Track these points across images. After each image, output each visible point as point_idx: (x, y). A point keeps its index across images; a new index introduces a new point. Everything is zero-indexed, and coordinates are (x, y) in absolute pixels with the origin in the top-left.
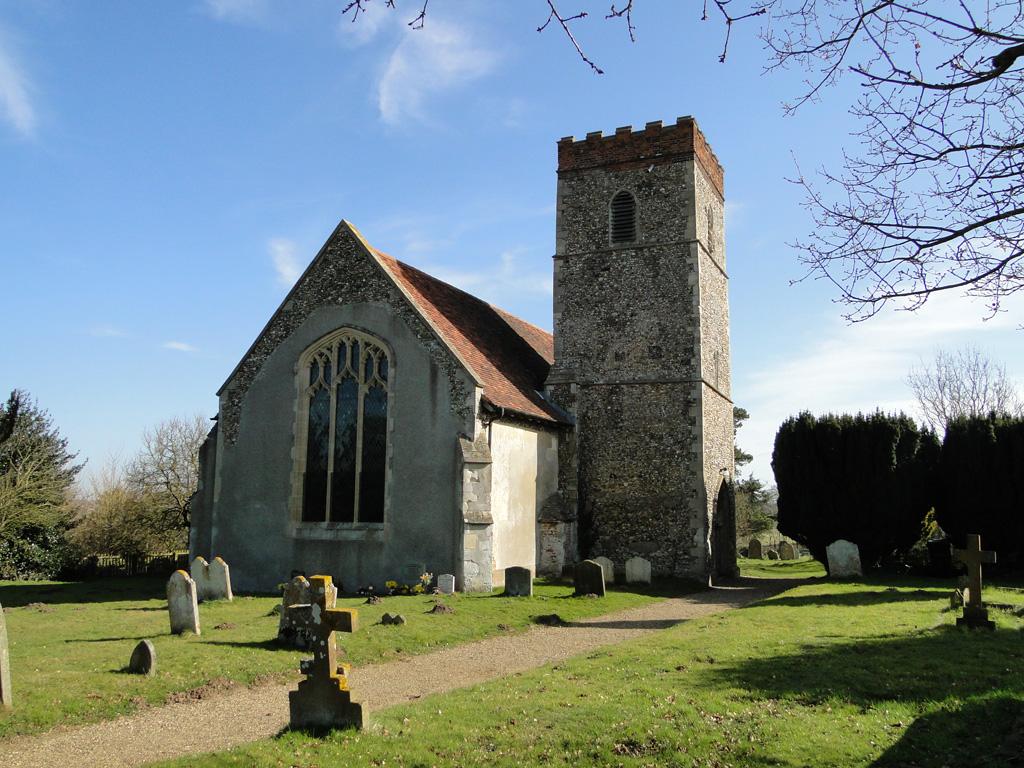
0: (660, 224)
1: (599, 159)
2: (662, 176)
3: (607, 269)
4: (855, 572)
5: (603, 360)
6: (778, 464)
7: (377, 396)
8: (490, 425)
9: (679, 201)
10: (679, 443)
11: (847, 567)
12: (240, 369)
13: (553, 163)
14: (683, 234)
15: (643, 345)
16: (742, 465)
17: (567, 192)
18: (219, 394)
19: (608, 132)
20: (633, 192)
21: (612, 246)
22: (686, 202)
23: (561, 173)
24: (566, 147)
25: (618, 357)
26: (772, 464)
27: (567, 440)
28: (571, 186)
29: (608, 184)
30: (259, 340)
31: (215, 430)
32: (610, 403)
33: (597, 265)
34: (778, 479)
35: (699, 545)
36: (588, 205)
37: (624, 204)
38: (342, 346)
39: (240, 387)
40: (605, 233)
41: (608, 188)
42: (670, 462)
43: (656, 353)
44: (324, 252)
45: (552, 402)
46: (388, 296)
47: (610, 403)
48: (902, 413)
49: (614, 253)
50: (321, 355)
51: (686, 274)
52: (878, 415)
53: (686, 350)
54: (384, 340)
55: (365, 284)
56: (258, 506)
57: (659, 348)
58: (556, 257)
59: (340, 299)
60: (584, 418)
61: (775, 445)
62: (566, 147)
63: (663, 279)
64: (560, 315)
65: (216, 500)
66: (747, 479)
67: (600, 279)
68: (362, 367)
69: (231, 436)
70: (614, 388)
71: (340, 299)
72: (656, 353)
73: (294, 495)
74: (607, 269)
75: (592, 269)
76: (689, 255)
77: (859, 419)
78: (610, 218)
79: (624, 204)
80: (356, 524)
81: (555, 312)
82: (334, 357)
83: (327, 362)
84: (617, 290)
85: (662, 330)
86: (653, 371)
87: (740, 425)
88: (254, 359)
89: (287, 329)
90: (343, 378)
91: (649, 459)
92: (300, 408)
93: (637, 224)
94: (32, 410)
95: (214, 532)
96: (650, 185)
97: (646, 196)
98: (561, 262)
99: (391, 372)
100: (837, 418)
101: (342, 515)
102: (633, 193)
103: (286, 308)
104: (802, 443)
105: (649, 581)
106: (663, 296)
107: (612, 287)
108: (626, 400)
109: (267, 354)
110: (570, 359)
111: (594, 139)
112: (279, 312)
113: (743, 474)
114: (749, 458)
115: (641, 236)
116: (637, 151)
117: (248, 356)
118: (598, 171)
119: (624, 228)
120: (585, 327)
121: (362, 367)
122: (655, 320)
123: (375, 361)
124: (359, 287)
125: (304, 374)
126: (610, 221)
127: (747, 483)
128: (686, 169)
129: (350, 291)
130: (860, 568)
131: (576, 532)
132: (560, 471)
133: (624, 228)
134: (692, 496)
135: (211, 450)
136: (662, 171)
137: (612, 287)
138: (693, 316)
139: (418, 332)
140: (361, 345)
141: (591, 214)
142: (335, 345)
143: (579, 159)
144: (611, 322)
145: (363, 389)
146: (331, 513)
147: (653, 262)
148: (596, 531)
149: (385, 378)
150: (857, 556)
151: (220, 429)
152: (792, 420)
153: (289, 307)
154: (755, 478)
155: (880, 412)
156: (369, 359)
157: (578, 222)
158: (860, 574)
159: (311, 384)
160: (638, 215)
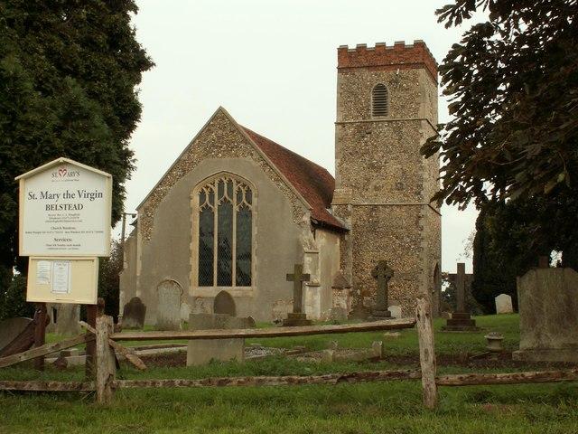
0: (403, 107)
7: (245, 214)
12: (152, 194)
13: (333, 61)
15: (391, 181)
19: (371, 45)
20: (386, 85)
21: (373, 119)
23: (340, 69)
24: (343, 51)
25: (376, 188)
26: (141, 63)
28: (345, 78)
29: (370, 78)
30: (165, 177)
32: (371, 216)
33: (363, 130)
37: (380, 91)
39: (151, 205)
40: (369, 110)
43: (400, 187)
44: (208, 125)
46: (252, 155)
47: (371, 216)
50: (207, 187)
53: (418, 186)
55: (237, 147)
58: (337, 124)
60: (355, 226)
64: (339, 161)
68: (235, 196)
69: (147, 236)
70: (375, 208)
72: (400, 187)
73: (193, 271)
74: (370, 133)
79: (380, 91)
81: (336, 158)
82: (216, 190)
83: (212, 192)
84: (376, 146)
85: (404, 173)
86: (396, 199)
89: (184, 171)
90: (240, 207)
91: (394, 251)
93: (389, 105)
96: (397, 82)
99: (255, 200)
101: (225, 280)
106: (404, 152)
107: (373, 144)
108: (382, 215)
110: (346, 189)
111: (361, 49)
112: (179, 161)
117: (157, 186)
119: (380, 108)
120: (357, 171)
121: (235, 196)
122: (399, 166)
123: (244, 192)
124: (232, 148)
125: (196, 199)
132: (341, 258)
133: (380, 108)
136: (405, 73)
137: (373, 144)
140: (235, 182)
142: (217, 181)
144: (372, 166)
147: (398, 130)
149: (250, 202)
153: (185, 157)
156: (239, 192)
157: (351, 101)
160: (389, 100)
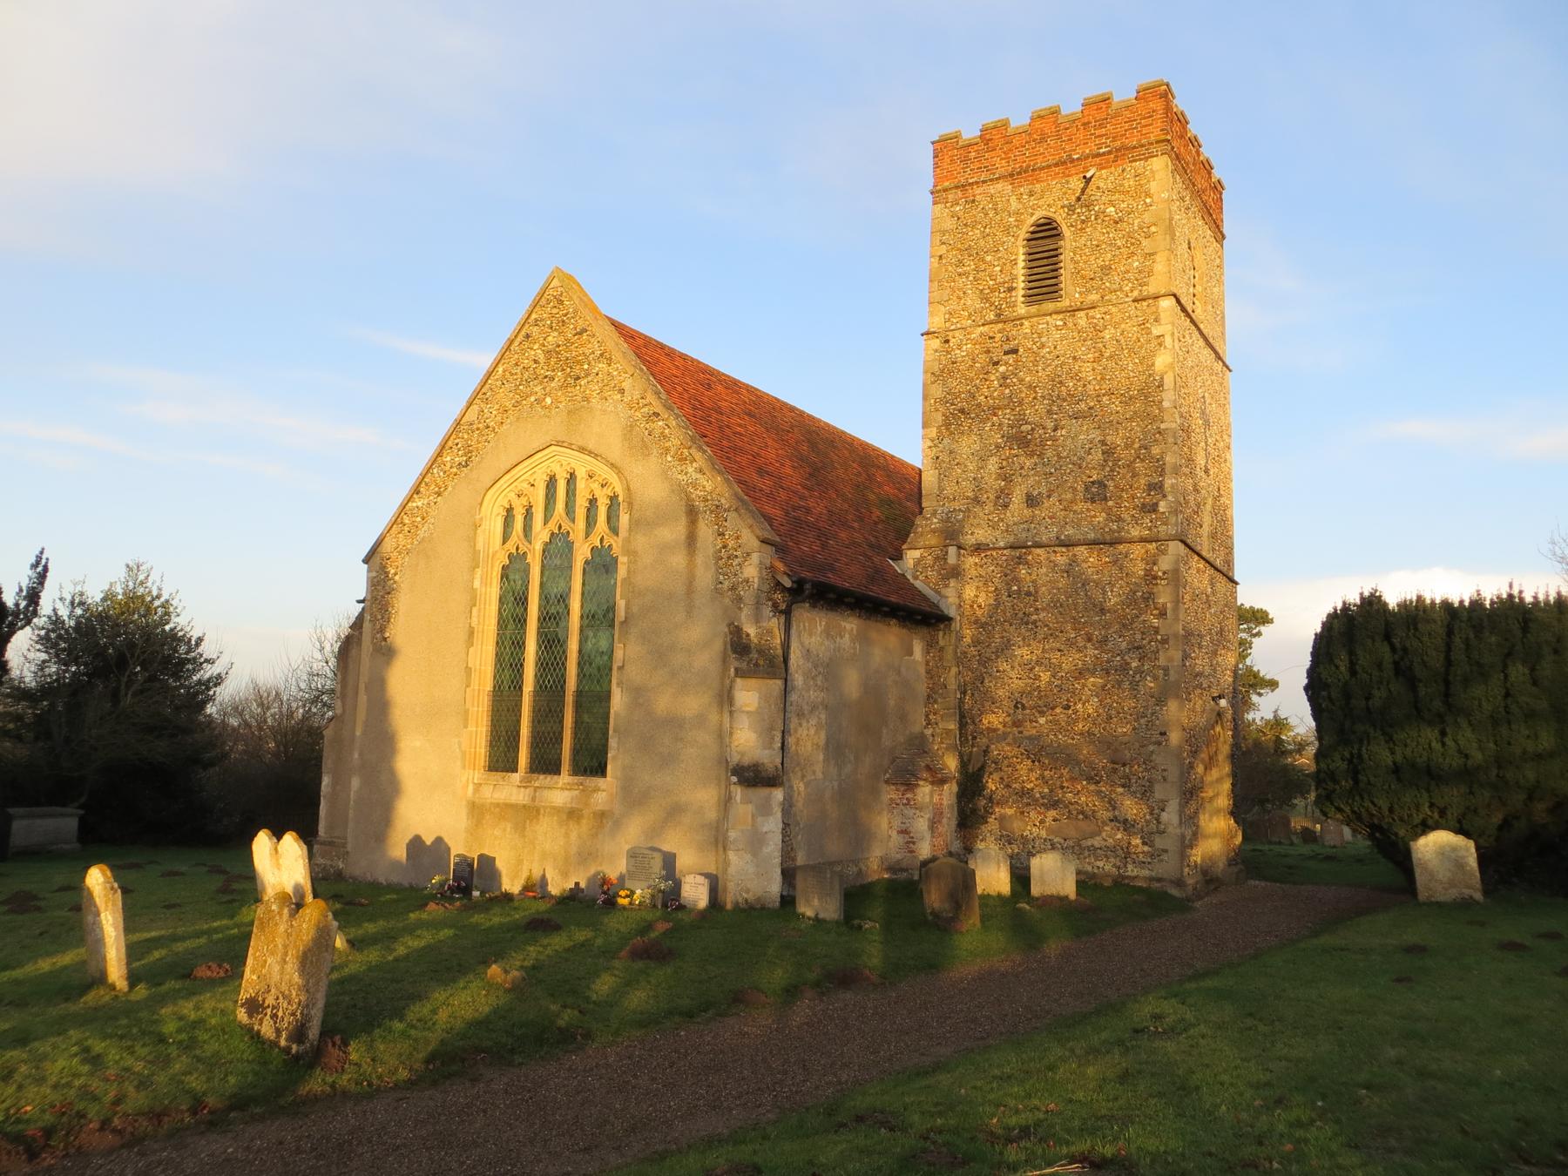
1: (1002, 167)
2: (1110, 186)
3: (1015, 351)
4: (1467, 892)
5: (1006, 506)
6: (1315, 688)
8: (787, 613)
9: (1141, 228)
10: (1138, 648)
11: (1452, 884)
14: (1146, 284)
16: (1260, 695)
17: (950, 224)
18: (366, 561)
20: (1060, 217)
21: (1022, 310)
22: (1153, 229)
24: (946, 148)
26: (1306, 689)
27: (941, 643)
31: (360, 618)
34: (1316, 714)
35: (1170, 829)
36: (982, 243)
38: (551, 483)
40: (1011, 289)
41: (1017, 213)
42: (1119, 683)
45: (916, 578)
48: (1559, 594)
49: (1026, 323)
51: (1153, 354)
52: (1511, 596)
54: (613, 466)
56: (418, 744)
57: (1101, 484)
59: (548, 400)
61: (1313, 654)
62: (946, 148)
63: (1111, 364)
65: (358, 733)
66: (1270, 716)
67: (1002, 369)
71: (548, 400)
74: (1015, 351)
75: (988, 352)
76: (1156, 320)
77: (1477, 604)
78: (1021, 264)
79: (1046, 231)
80: (565, 778)
87: (1259, 634)
88: (418, 502)
92: (484, 583)
94: (155, 593)
95: (355, 783)
97: (1083, 222)
98: (936, 343)
100: (1433, 602)
102: (1059, 219)
103: (468, 418)
104: (1359, 643)
105: (1073, 896)
109: (439, 494)
113: (1263, 708)
114: (1273, 684)
115: (1071, 291)
116: (1068, 148)
118: (999, 186)
126: (1020, 270)
127: (893, 868)
128: (1152, 171)
129: (564, 386)
130: (1479, 886)
131: (954, 799)
134: (1159, 744)
135: (354, 652)
138: (1163, 426)
139: (667, 450)
140: (581, 474)
141: (988, 258)
143: (963, 164)
145: (582, 553)
146: (576, 752)
148: (990, 799)
150: (1472, 861)
151: (367, 617)
152: (1346, 607)
153: (472, 415)
154: (1282, 715)
155: (1515, 592)
156: (593, 502)
157: (966, 274)
158: (1478, 896)
159: (505, 540)
